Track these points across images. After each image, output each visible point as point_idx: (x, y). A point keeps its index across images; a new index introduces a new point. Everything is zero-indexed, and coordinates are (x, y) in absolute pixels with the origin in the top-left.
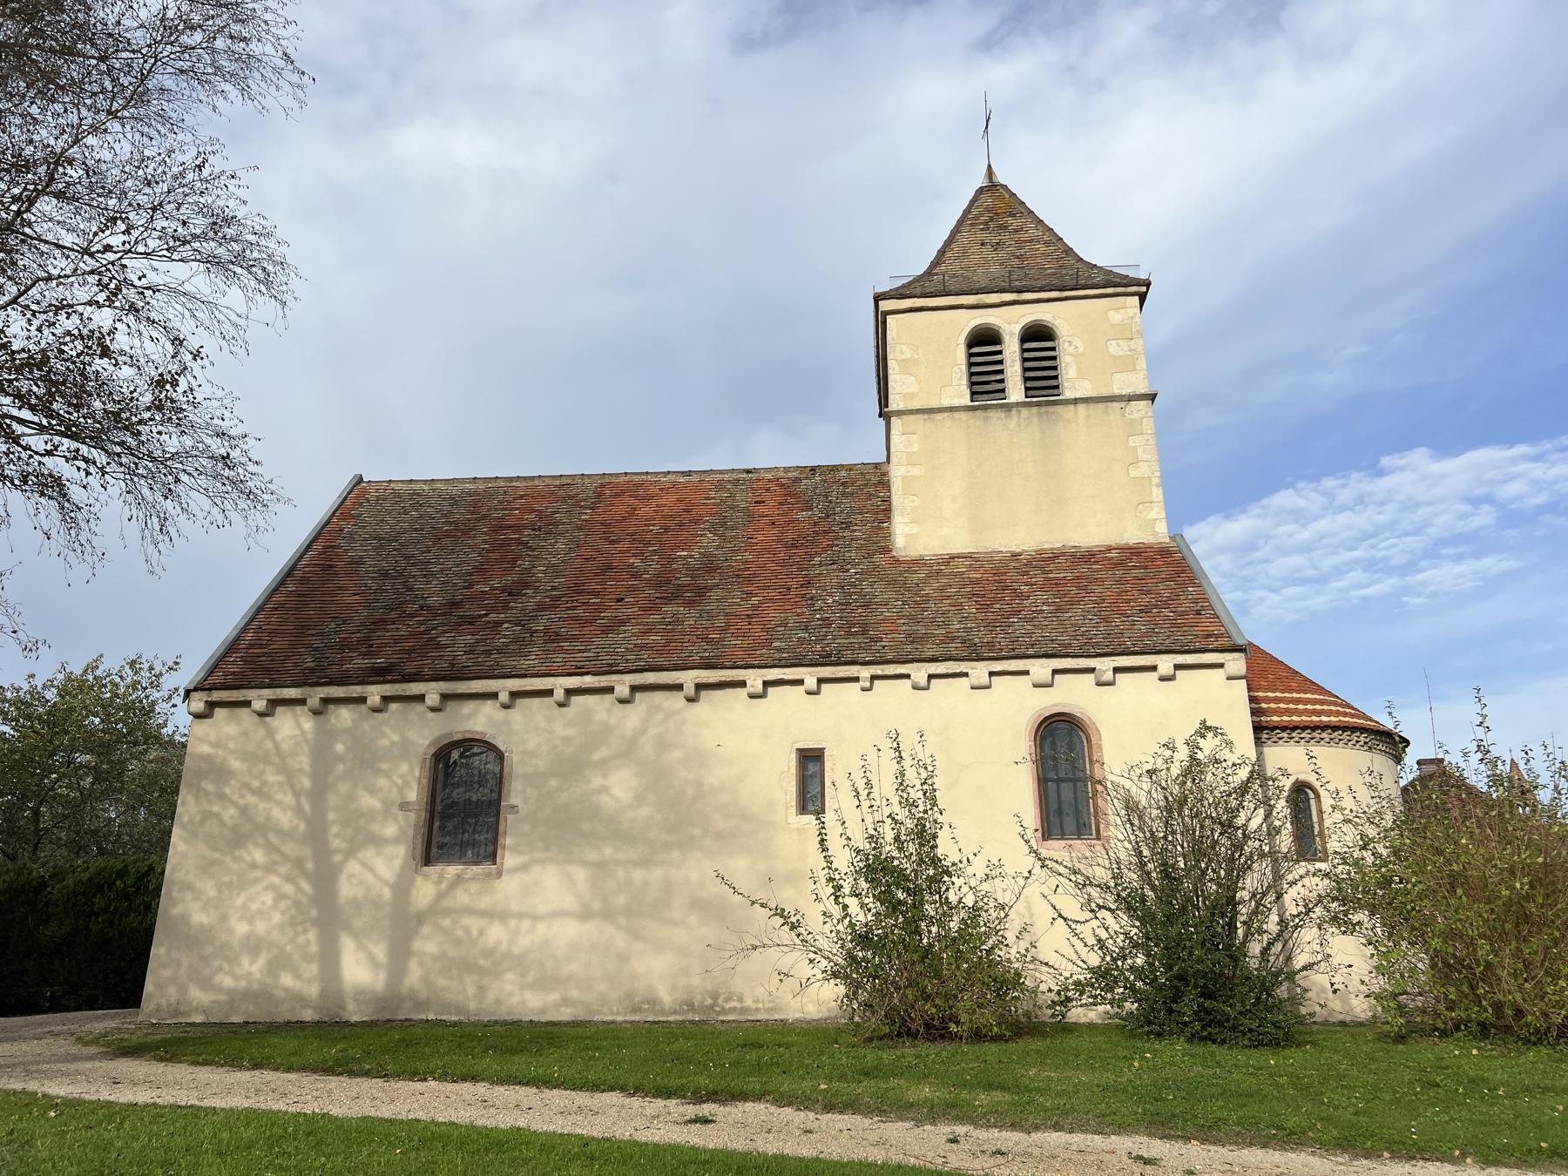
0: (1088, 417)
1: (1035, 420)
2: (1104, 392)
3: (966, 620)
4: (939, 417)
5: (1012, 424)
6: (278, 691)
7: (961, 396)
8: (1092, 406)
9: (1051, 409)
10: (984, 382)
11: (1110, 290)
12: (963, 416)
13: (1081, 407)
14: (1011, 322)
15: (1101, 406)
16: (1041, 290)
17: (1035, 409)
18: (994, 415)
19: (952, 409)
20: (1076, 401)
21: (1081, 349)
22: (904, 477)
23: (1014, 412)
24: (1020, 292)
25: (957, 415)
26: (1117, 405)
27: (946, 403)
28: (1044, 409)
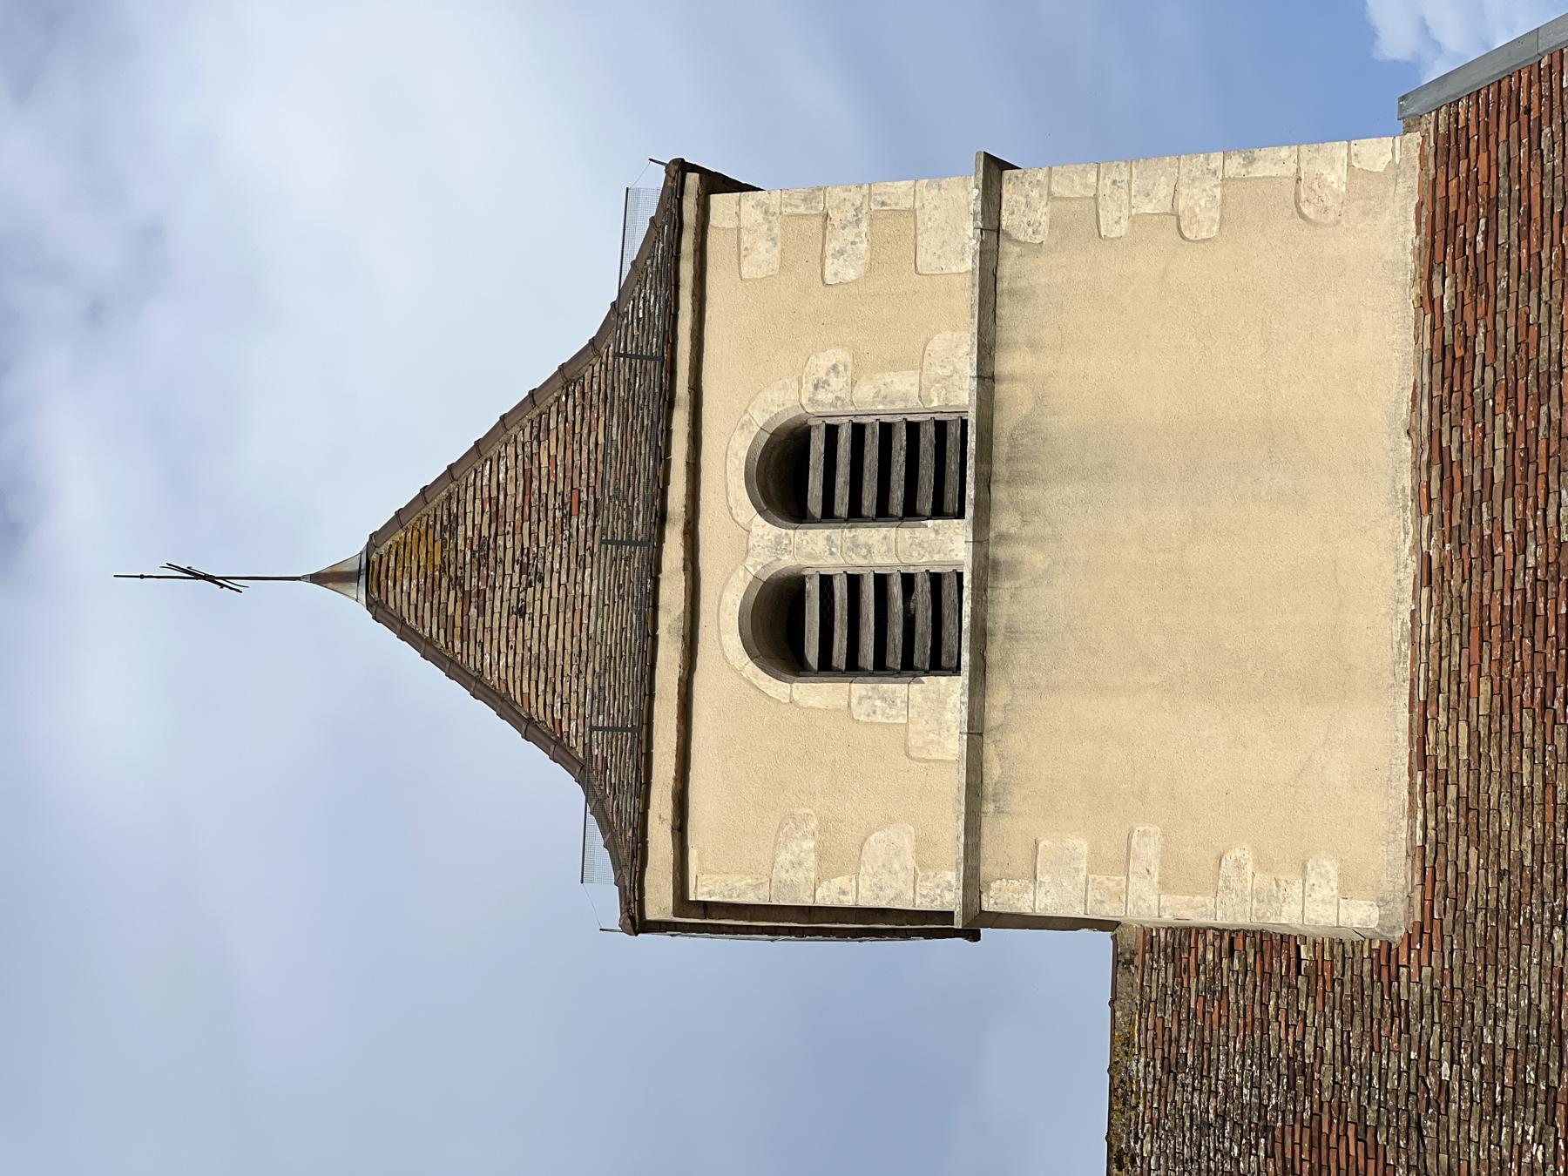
0: (1034, 346)
2: (965, 299)
4: (994, 770)
5: (1034, 559)
7: (941, 702)
8: (1003, 335)
9: (1001, 449)
12: (998, 697)
16: (663, 457)
19: (976, 732)
23: (1001, 553)
24: (662, 517)
25: (994, 717)
27: (954, 746)
28: (1000, 468)
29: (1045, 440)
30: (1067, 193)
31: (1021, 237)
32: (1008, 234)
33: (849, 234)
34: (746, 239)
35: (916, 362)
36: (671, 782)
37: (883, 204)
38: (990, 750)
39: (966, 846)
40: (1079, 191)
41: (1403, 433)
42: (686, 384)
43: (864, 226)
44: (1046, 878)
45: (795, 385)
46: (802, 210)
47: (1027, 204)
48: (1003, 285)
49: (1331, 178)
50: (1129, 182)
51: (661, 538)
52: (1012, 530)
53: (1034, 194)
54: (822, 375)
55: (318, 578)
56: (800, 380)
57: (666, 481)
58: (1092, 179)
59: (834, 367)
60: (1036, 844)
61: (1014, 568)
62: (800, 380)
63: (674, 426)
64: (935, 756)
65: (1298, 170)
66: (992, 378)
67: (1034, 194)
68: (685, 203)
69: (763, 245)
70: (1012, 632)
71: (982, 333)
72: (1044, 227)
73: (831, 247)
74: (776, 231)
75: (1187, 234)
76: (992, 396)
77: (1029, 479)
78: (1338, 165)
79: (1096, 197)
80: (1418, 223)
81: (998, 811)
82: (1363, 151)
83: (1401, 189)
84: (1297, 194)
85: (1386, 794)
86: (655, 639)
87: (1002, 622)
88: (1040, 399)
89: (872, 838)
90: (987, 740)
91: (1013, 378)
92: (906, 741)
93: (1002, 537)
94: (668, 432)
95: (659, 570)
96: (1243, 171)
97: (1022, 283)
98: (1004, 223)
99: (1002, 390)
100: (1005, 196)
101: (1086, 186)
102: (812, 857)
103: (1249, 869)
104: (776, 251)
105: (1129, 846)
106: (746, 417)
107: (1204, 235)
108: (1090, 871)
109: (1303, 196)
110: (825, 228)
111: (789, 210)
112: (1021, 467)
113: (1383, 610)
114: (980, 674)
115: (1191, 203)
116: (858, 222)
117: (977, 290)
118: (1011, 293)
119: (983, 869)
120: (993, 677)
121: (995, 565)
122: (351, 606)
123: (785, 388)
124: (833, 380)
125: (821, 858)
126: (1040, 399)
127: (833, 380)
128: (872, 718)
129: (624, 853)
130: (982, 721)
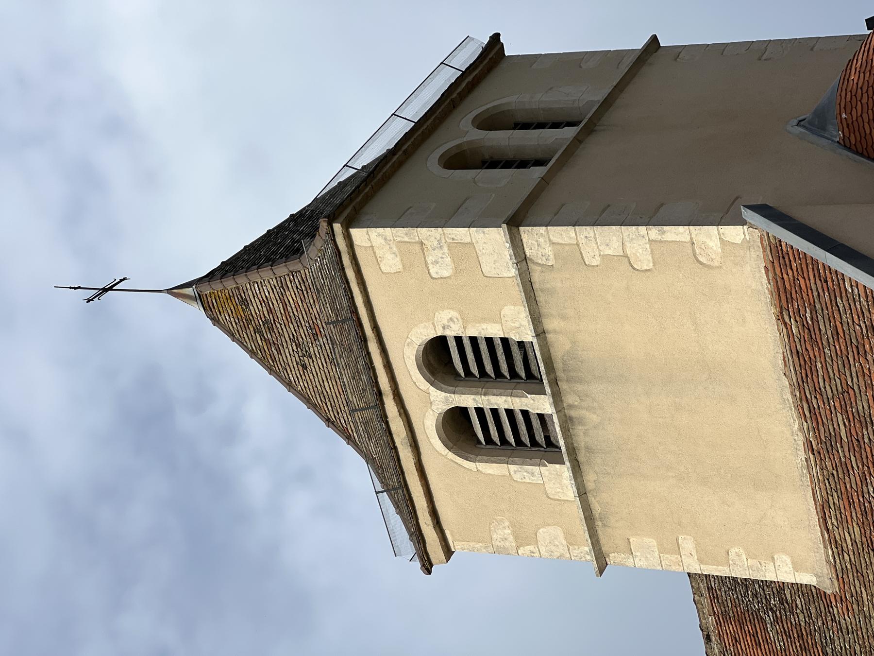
0: (563, 317)
1: (579, 387)
2: (517, 292)
3: (587, 514)
4: (597, 509)
5: (593, 418)
6: (501, 348)
7: (559, 475)
8: (544, 310)
9: (558, 365)
10: (531, 440)
11: (346, 260)
12: (590, 478)
13: (550, 324)
14: (428, 403)
15: (541, 298)
16: (371, 367)
17: (563, 386)
18: (560, 346)
19: (582, 493)
20: (536, 319)
21: (454, 314)
22: (701, 561)
23: (573, 413)
24: (380, 394)
25: (590, 485)
26: (537, 277)
27: (571, 493)
28: (560, 374)
29: (582, 362)
30: (560, 241)
31: (540, 262)
32: (531, 260)
33: (439, 253)
34: (379, 253)
35: (497, 319)
36: (427, 509)
37: (453, 239)
38: (591, 499)
39: (592, 543)
40: (566, 240)
41: (782, 375)
42: (370, 329)
43: (446, 250)
44: (638, 554)
45: (431, 326)
46: (406, 239)
47: (539, 245)
48: (536, 286)
49: (711, 244)
50: (595, 238)
51: (383, 403)
52: (576, 403)
53: (541, 240)
54: (445, 322)
55: (169, 291)
56: (433, 324)
57: (376, 377)
58: (573, 235)
59: (451, 319)
60: (629, 540)
61: (581, 421)
62: (433, 324)
63: (371, 350)
64: (563, 498)
65: (691, 239)
66: (544, 332)
67: (541, 240)
68: (337, 240)
69: (389, 256)
70: (588, 449)
71: (532, 314)
72: (551, 257)
73: (430, 259)
74: (395, 249)
75: (635, 266)
76: (546, 340)
77: (580, 380)
78: (714, 238)
79: (577, 244)
80: (768, 279)
81: (604, 525)
82: (727, 232)
83: (754, 255)
84: (694, 251)
85: (809, 531)
86: (395, 448)
87: (582, 444)
88: (574, 343)
89: (540, 531)
90: (589, 495)
91: (555, 332)
92: (546, 493)
93: (571, 406)
94: (368, 354)
95: (386, 417)
96: (660, 237)
97: (548, 286)
98: (528, 254)
99: (551, 337)
100: (524, 240)
101: (570, 238)
102: (511, 537)
103: (744, 557)
104: (398, 259)
105: (678, 543)
106: (409, 340)
107: (646, 268)
108: (660, 552)
109: (698, 251)
110: (423, 250)
111: (399, 239)
112: (571, 374)
113: (789, 452)
114: (577, 468)
115: (634, 251)
116: (441, 247)
117: (523, 294)
118: (542, 290)
119: (603, 549)
120: (584, 468)
121: (571, 419)
122: (196, 311)
123: (425, 327)
124: (452, 324)
125: (516, 538)
126: (574, 343)
127: (452, 324)
128: (524, 480)
129: (405, 510)
130: (584, 487)
